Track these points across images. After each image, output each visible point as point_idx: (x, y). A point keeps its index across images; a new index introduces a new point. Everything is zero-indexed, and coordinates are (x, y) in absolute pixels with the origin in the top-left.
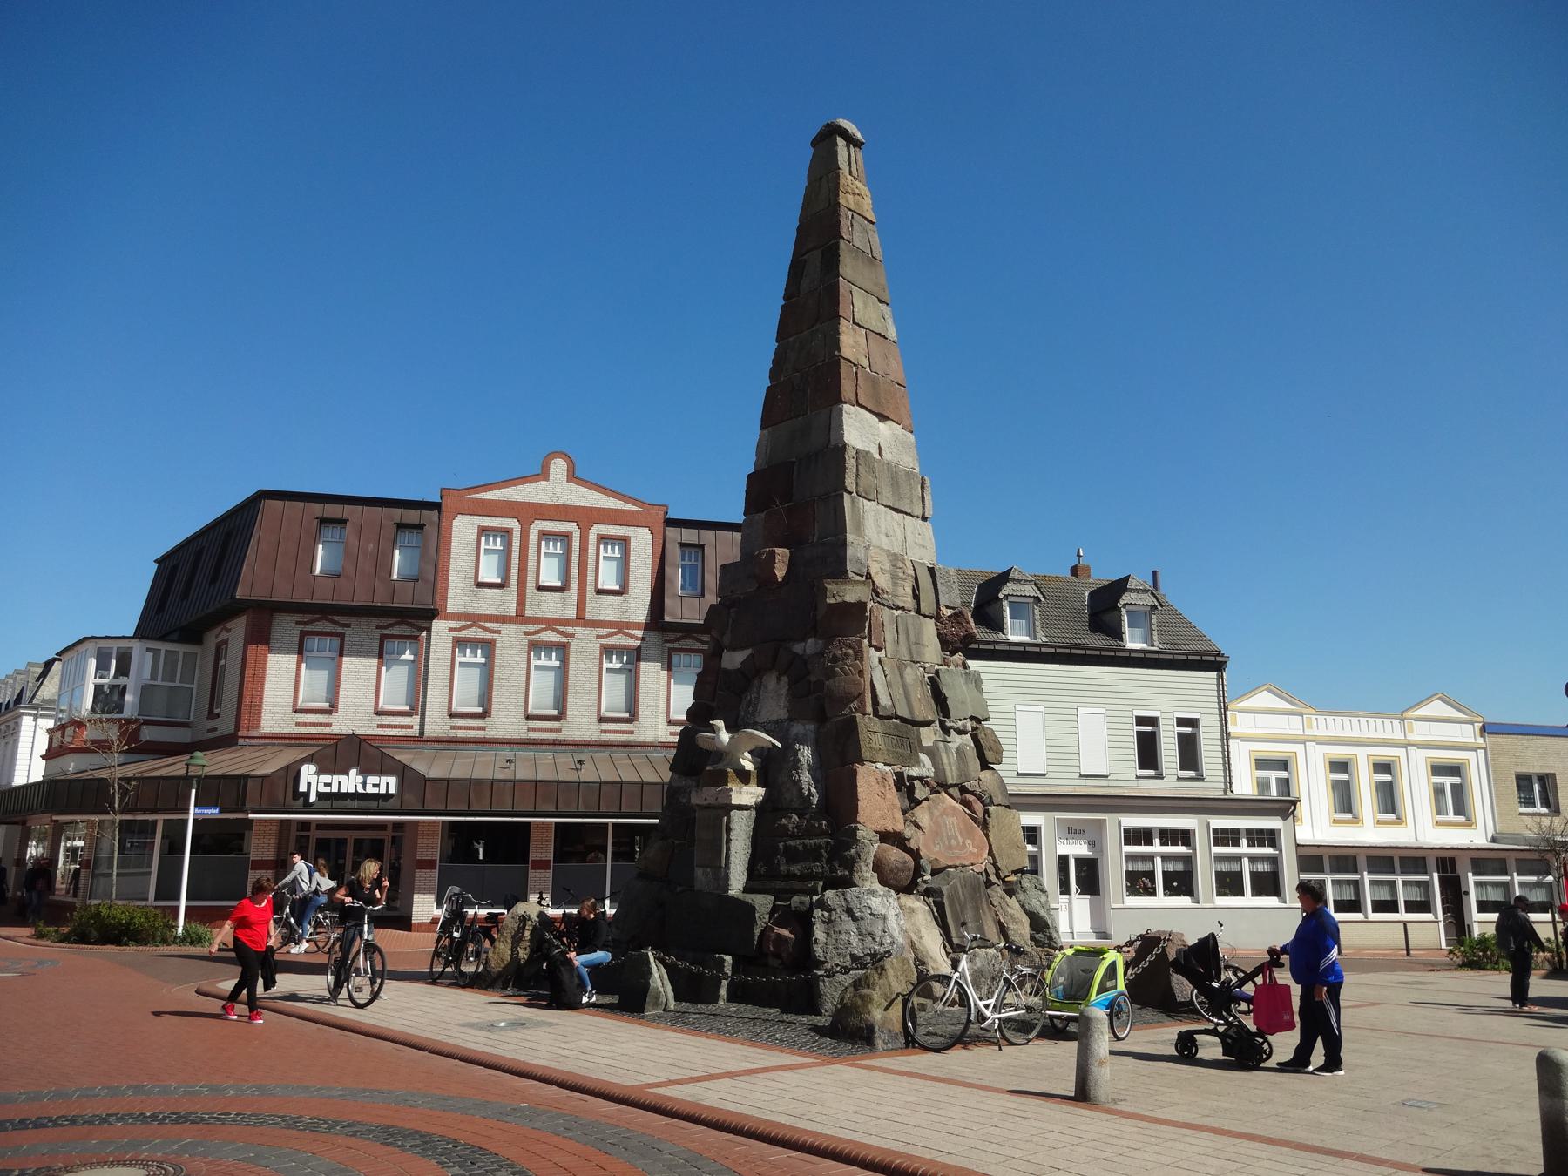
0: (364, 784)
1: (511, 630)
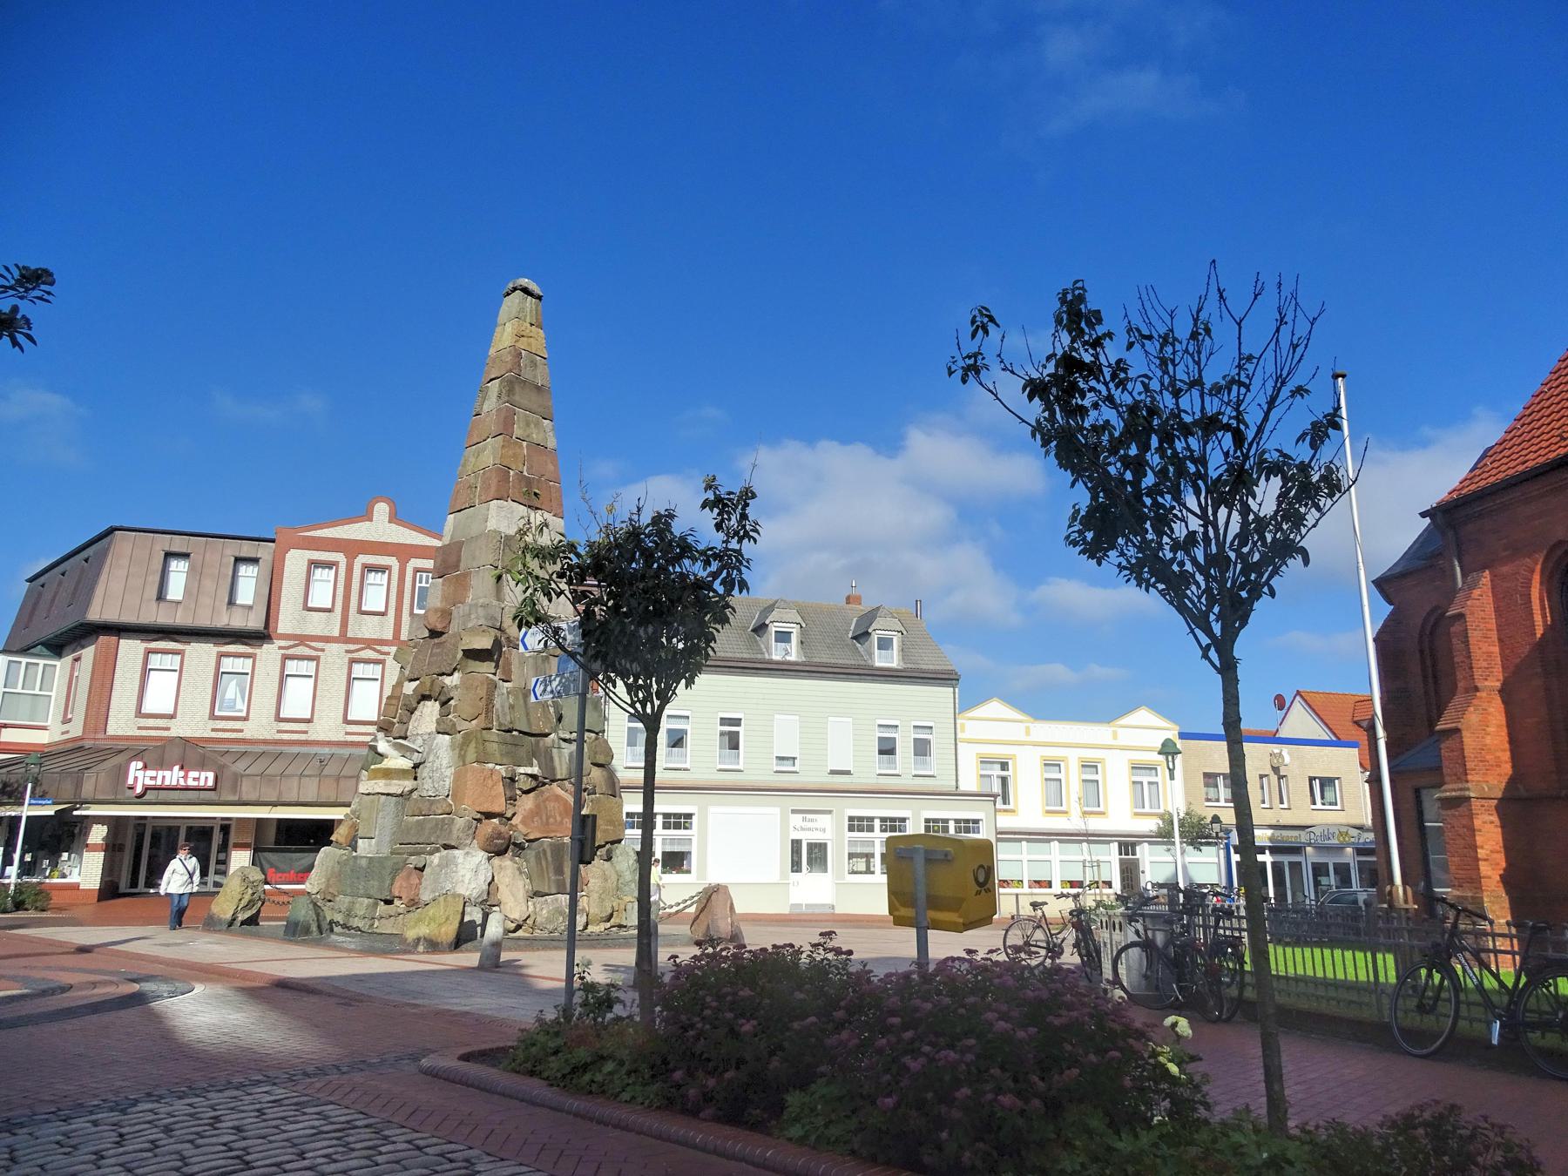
0: (185, 777)
1: (335, 649)
